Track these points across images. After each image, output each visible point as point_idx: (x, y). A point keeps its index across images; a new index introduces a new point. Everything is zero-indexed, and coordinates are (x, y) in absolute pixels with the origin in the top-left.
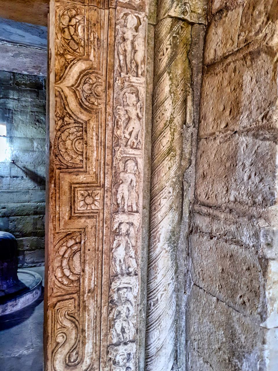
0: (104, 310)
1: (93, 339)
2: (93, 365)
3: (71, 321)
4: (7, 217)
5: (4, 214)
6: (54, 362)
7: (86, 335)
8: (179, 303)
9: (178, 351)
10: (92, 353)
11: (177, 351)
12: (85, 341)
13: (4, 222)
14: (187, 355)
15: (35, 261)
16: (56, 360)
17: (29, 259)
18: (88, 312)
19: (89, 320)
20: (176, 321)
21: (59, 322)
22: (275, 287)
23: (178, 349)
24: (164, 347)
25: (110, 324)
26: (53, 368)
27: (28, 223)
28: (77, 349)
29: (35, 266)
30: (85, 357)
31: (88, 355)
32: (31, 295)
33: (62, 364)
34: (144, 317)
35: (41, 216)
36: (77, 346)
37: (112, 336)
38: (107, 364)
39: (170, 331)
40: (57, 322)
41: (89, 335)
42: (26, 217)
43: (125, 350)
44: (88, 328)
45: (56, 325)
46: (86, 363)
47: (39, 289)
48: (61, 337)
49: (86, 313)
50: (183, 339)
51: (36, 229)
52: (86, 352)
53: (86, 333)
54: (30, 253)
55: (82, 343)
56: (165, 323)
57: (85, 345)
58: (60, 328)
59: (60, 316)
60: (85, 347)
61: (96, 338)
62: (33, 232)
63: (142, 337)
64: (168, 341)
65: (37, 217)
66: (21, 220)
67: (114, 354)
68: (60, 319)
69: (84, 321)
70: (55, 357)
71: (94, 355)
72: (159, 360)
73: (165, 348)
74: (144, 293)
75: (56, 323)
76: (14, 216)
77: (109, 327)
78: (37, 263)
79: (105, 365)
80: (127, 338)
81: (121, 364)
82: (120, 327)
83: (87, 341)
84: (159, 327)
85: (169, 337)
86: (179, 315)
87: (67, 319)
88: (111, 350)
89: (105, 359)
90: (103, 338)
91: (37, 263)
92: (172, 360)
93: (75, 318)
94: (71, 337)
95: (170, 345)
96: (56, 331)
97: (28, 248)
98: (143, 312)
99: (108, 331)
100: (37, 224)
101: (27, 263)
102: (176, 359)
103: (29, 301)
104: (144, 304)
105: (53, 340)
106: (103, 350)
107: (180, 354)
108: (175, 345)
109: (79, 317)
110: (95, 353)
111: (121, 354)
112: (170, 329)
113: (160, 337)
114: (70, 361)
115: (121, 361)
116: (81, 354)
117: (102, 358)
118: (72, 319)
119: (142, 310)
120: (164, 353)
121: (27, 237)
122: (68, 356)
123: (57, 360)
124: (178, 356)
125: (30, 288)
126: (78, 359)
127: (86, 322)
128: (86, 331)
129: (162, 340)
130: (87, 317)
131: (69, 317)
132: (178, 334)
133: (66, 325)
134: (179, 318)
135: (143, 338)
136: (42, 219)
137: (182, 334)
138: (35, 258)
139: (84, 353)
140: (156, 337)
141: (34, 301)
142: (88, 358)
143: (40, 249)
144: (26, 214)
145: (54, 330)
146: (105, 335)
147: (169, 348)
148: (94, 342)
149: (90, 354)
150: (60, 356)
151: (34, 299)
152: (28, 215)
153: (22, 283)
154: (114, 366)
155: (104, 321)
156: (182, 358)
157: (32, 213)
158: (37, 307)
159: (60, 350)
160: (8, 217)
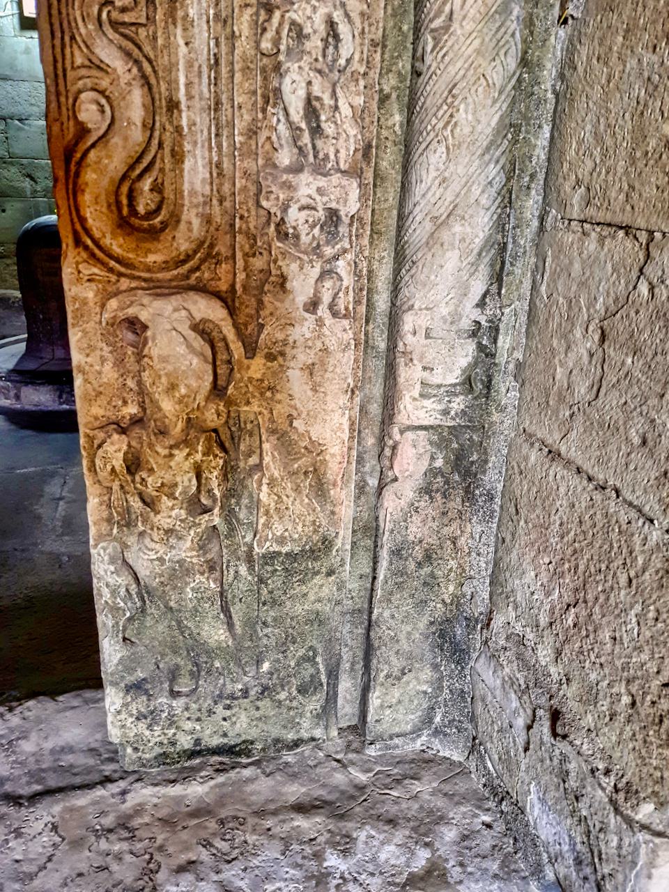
0: (243, 25)
1: (210, 148)
2: (212, 246)
3: (128, 54)
6: (80, 198)
7: (184, 122)
8: (534, 54)
9: (510, 246)
10: (208, 202)
11: (503, 248)
12: (181, 146)
14: (539, 269)
16: (83, 191)
18: (185, 30)
19: (190, 65)
20: (513, 129)
21: (78, 39)
23: (510, 240)
24: (459, 211)
25: (265, 87)
26: (76, 220)
28: (154, 173)
30: (183, 205)
31: (195, 201)
33: (104, 210)
34: (397, 128)
36: (152, 163)
37: (274, 138)
38: (259, 244)
39: (487, 157)
40: (73, 38)
41: (192, 124)
43: (320, 191)
44: (190, 97)
45: (68, 51)
46: (190, 230)
48: (94, 107)
49: (179, 31)
50: (531, 205)
52: (186, 187)
53: (184, 115)
55: (173, 153)
56: (470, 117)
57: (183, 162)
58: (84, 66)
59: (78, 14)
60: (182, 171)
61: (219, 146)
63: (386, 205)
64: (476, 190)
67: (277, 198)
68: (83, 31)
69: (172, 67)
70: (81, 181)
71: (216, 209)
72: (438, 261)
73: (463, 218)
74: (405, 28)
75: (67, 39)
77: (263, 96)
79: (252, 246)
80: (327, 157)
81: (305, 239)
82: (302, 93)
83: (187, 147)
84: (448, 132)
85: (483, 180)
86: (528, 108)
87: (111, 41)
88: (269, 183)
89: (251, 226)
90: (242, 139)
92: (484, 271)
93: (140, 48)
94: (128, 114)
95: (482, 212)
96: (70, 74)
98: (395, 107)
99: (260, 116)
102: (498, 277)
104: (399, 73)
105: (64, 109)
106: (244, 189)
107: (515, 257)
108: (500, 225)
109: (154, 48)
110: (221, 202)
111: (304, 201)
112: (488, 149)
113: (446, 174)
114: (132, 205)
115: (304, 230)
116: (172, 197)
117: (242, 217)
118: (130, 46)
119: (394, 96)
120: (458, 237)
122: (125, 189)
123: (88, 190)
124: (507, 265)
126: (163, 212)
127: (181, 67)
128: (183, 107)
129: (455, 186)
130: (183, 50)
131: (117, 36)
132: (514, 182)
133: (107, 61)
134: (526, 118)
135: (389, 210)
137: (528, 188)
139: (182, 191)
140: (433, 174)
142: (194, 211)
145: (64, 70)
146: (250, 130)
147: (479, 226)
148: (215, 159)
149: (201, 199)
150: (94, 176)
154: (279, 244)
155: (242, 70)
156: (520, 273)
159: (92, 155)
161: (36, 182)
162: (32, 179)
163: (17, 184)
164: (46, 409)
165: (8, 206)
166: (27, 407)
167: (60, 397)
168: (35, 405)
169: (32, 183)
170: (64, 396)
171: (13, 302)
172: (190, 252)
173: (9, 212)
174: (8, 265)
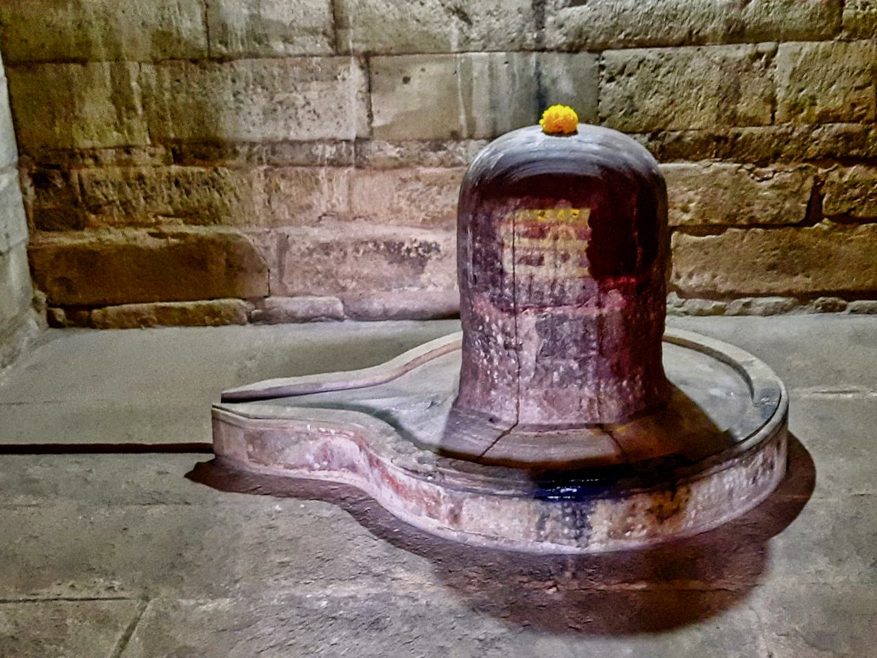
4: (591, 51)
5: (580, 33)
13: (575, 80)
15: (723, 288)
17: (690, 276)
22: (6, 190)
27: (691, 84)
29: (719, 312)
32: (744, 471)
35: (765, 47)
42: (683, 50)
47: (778, 445)
51: (734, 120)
54: (695, 245)
62: (718, 139)
65: (742, 51)
66: (658, 67)
76: (625, 45)
78: (733, 295)
91: (733, 295)
97: (686, 217)
100: (738, 95)
101: (681, 293)
103: (736, 500)
121: (687, 158)
125: (739, 435)
136: (767, 64)
138: (721, 274)
141: (755, 501)
143: (748, 227)
144: (683, 33)
151: (756, 492)
152: (694, 40)
153: (689, 404)
157: (714, 32)
158: (778, 543)
160: (597, 50)
161: (470, 23)
162: (464, 17)
163: (435, 30)
164: (508, 547)
165: (415, 73)
166: (472, 539)
167: (540, 526)
168: (487, 537)
169: (462, 23)
170: (549, 525)
171: (409, 250)
172: (340, 32)
173: (415, 83)
174: (404, 181)
